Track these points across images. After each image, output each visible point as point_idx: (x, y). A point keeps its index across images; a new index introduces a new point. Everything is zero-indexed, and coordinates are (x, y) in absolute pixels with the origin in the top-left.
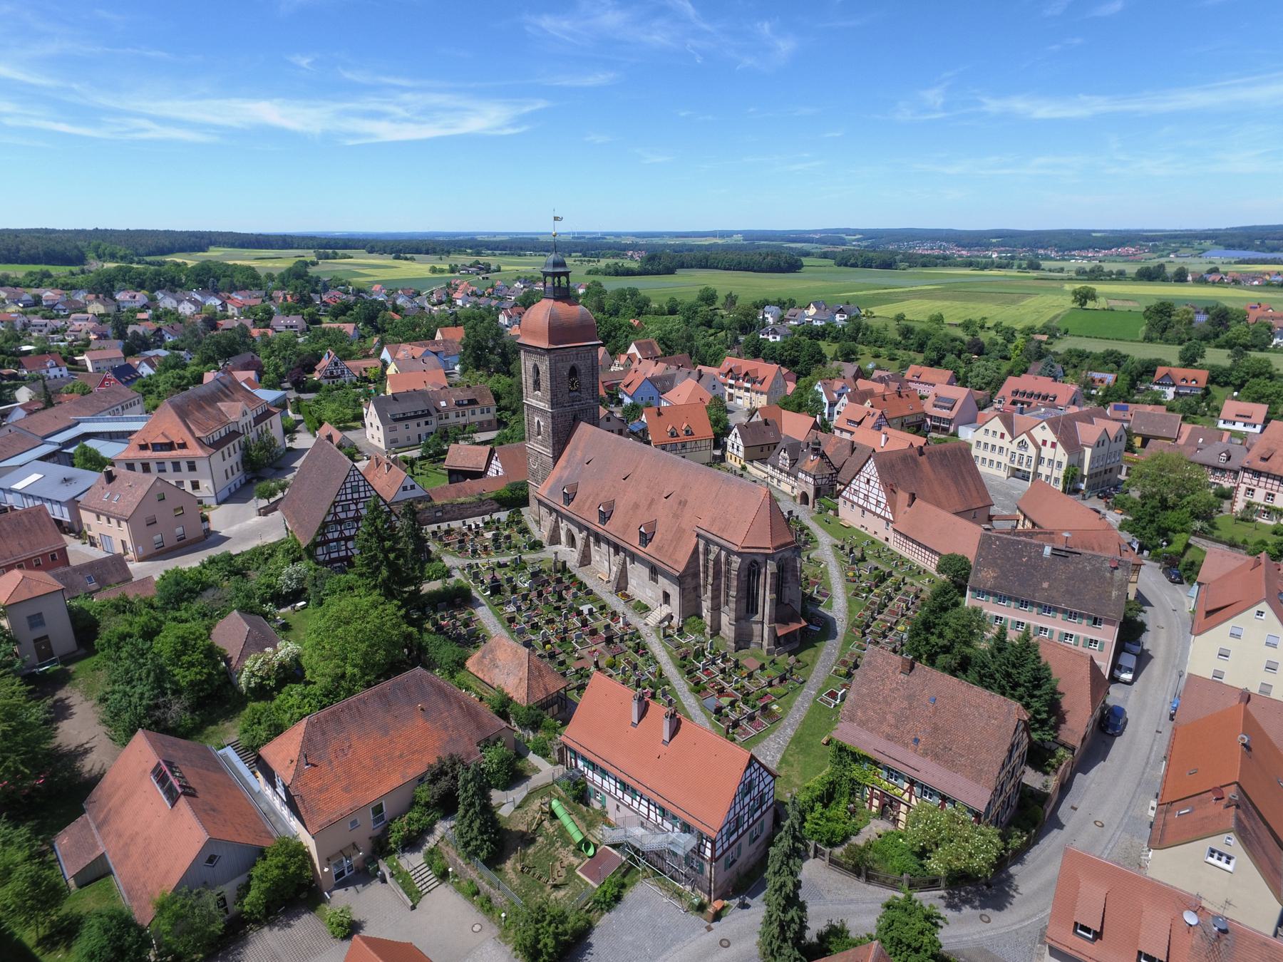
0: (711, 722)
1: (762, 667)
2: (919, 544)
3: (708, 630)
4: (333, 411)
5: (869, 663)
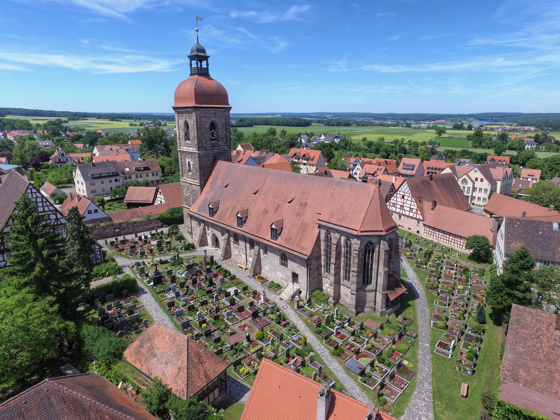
0: (359, 385)
1: (382, 328)
2: (444, 232)
3: (331, 300)
4: (53, 177)
5: (518, 322)
